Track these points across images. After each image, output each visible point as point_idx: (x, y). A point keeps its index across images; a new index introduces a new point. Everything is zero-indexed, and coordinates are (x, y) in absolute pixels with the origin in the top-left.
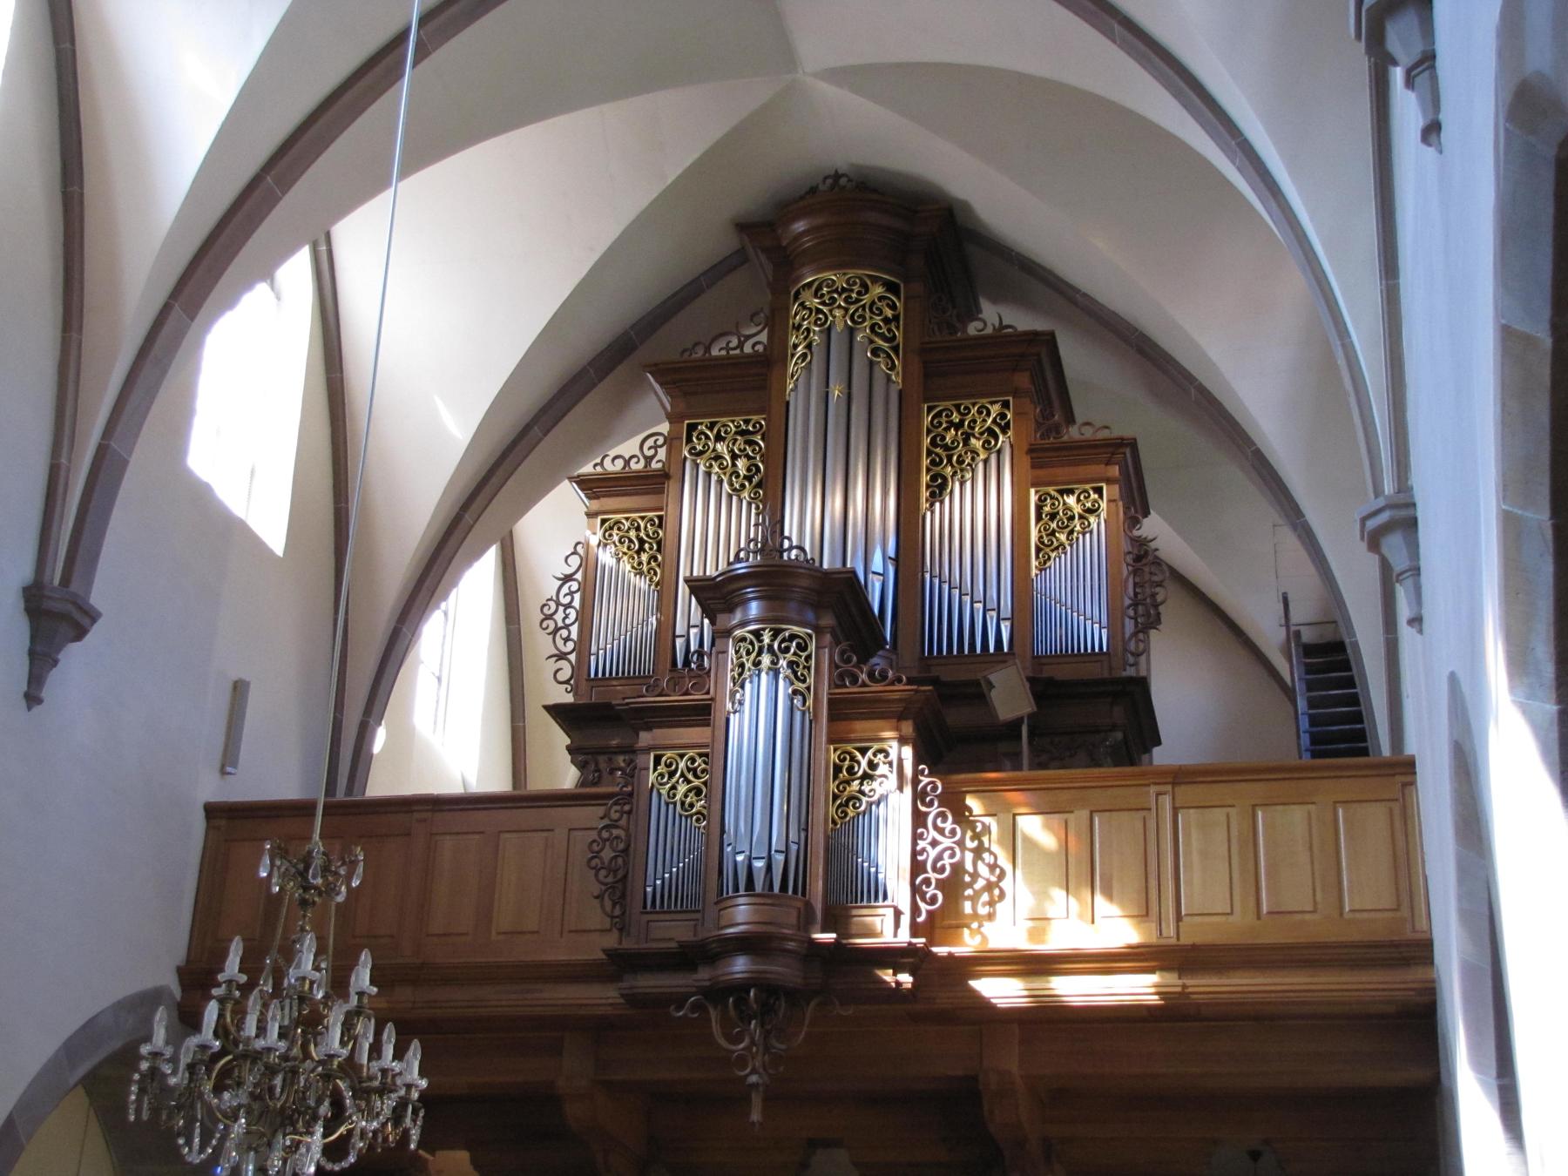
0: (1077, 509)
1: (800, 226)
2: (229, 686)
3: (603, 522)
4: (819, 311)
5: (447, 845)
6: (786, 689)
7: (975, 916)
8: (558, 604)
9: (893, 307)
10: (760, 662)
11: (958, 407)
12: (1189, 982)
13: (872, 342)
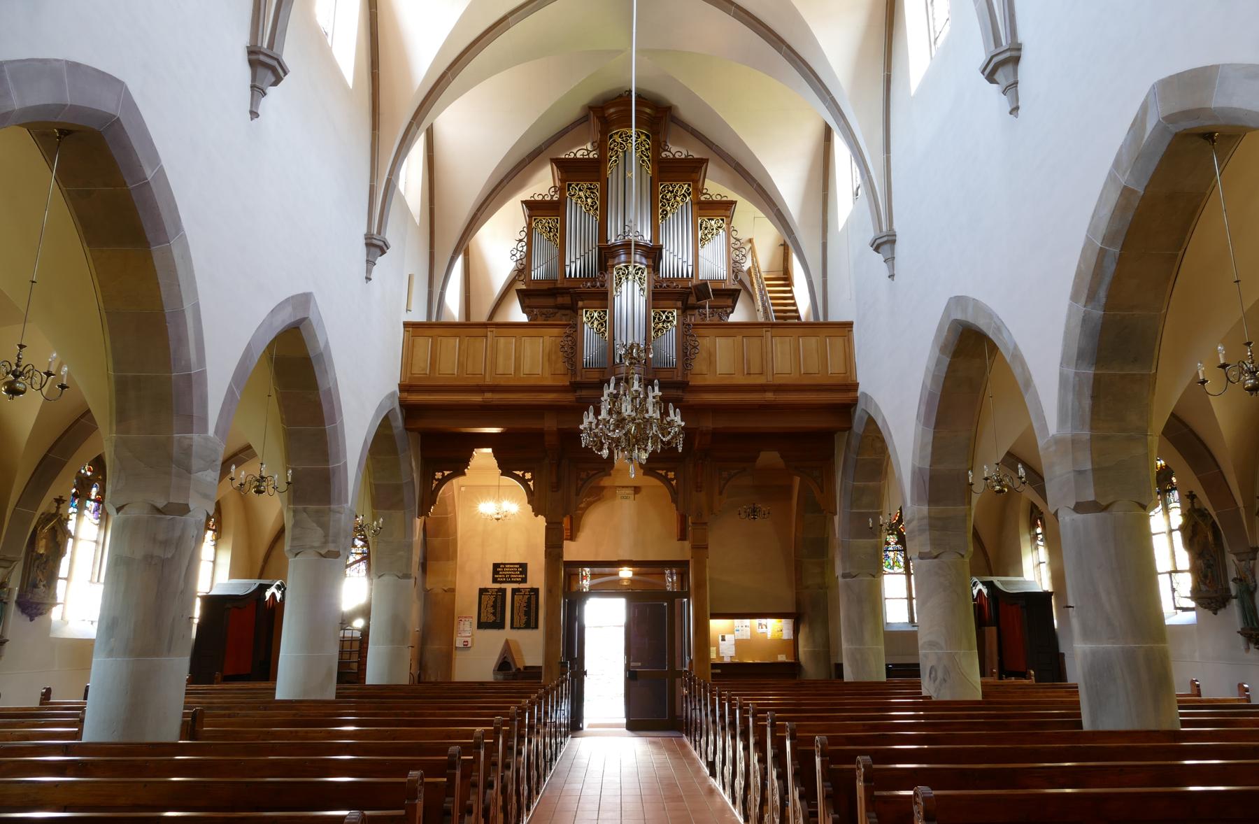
1: (612, 110)
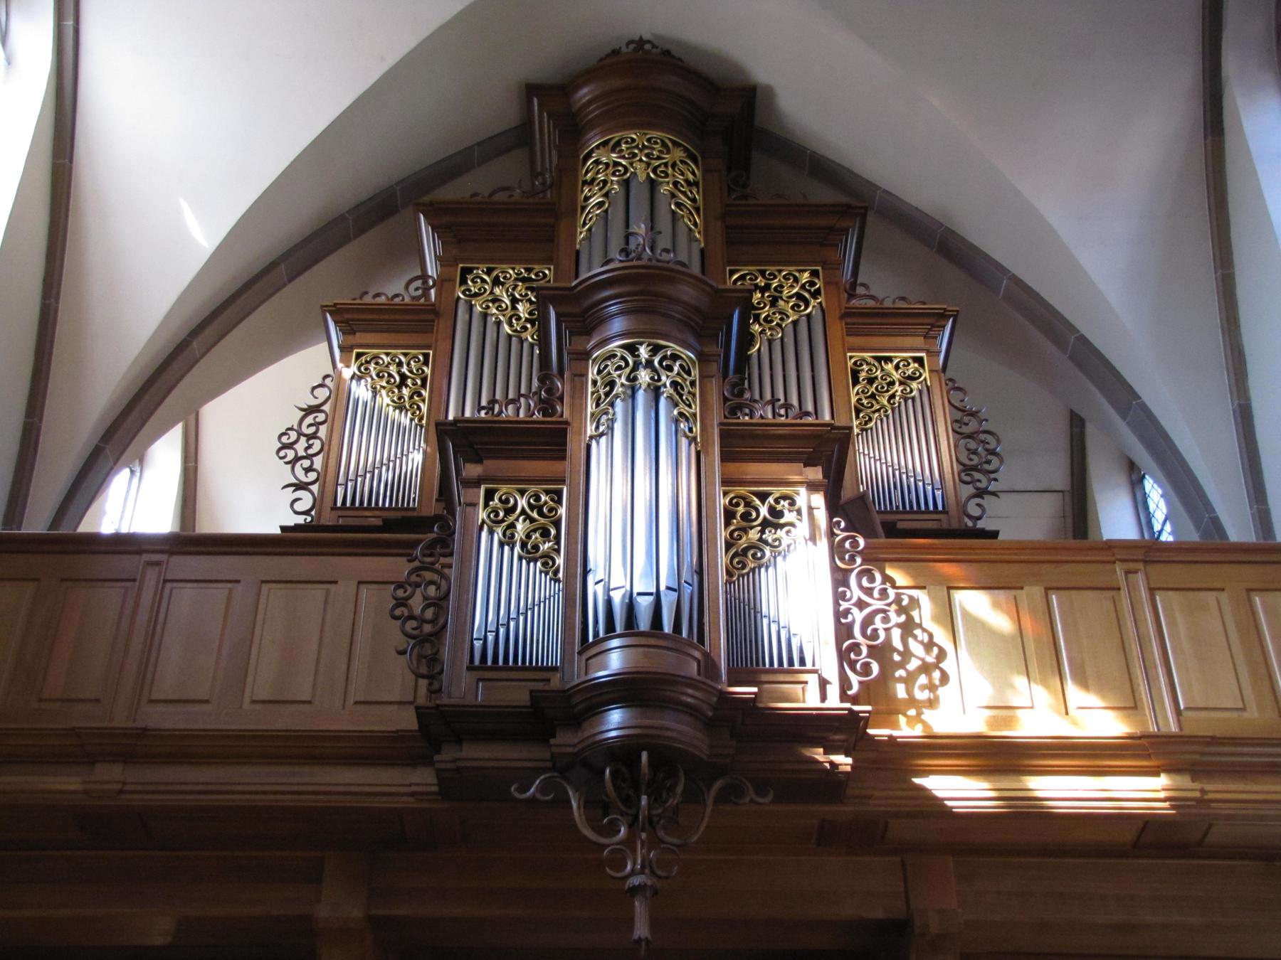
0: (896, 376)
3: (359, 356)
4: (616, 164)
5: (185, 599)
6: (669, 412)
7: (912, 701)
8: (300, 434)
9: (693, 173)
10: (635, 379)
12: (1208, 787)
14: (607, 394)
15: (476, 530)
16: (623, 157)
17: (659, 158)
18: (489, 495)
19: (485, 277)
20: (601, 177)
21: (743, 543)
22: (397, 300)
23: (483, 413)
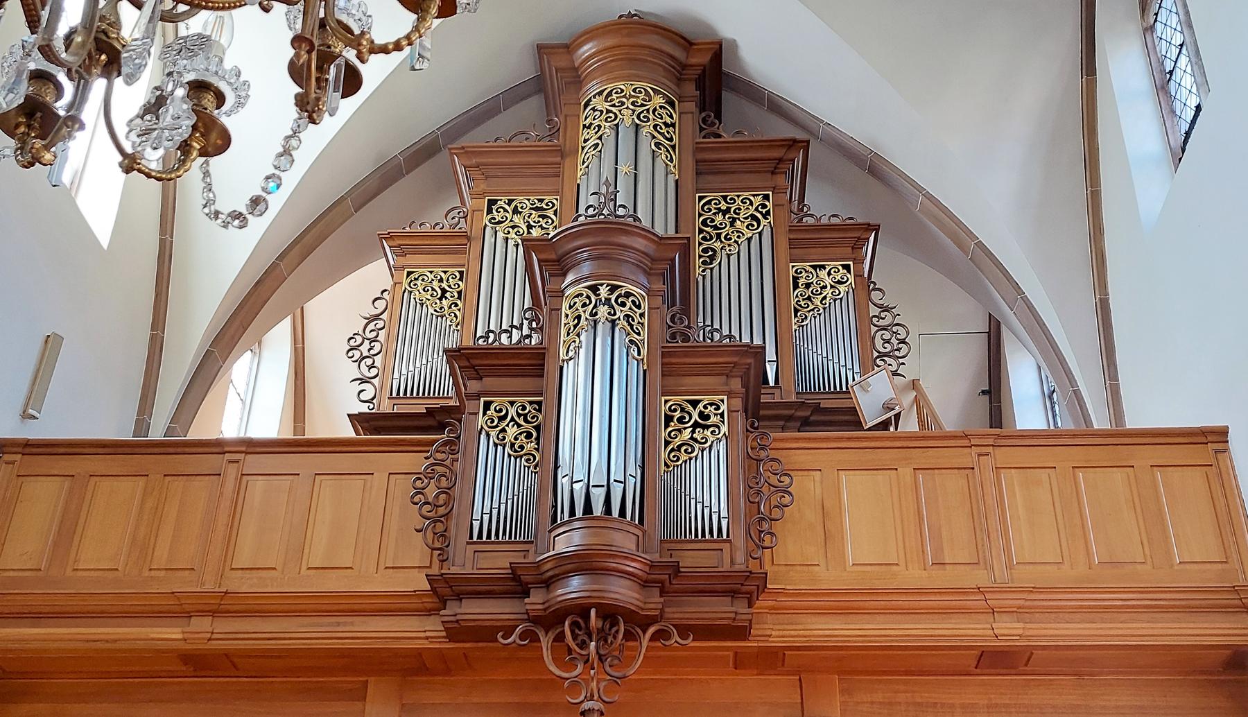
0: (828, 281)
2: (42, 340)
3: (409, 274)
4: (608, 111)
5: (258, 486)
9: (671, 116)
11: (725, 198)
13: (654, 137)
14: (575, 326)
15: (476, 434)
16: (614, 106)
17: (642, 105)
18: (487, 406)
19: (507, 207)
20: (596, 122)
21: (677, 442)
22: (438, 229)
23: (481, 342)
